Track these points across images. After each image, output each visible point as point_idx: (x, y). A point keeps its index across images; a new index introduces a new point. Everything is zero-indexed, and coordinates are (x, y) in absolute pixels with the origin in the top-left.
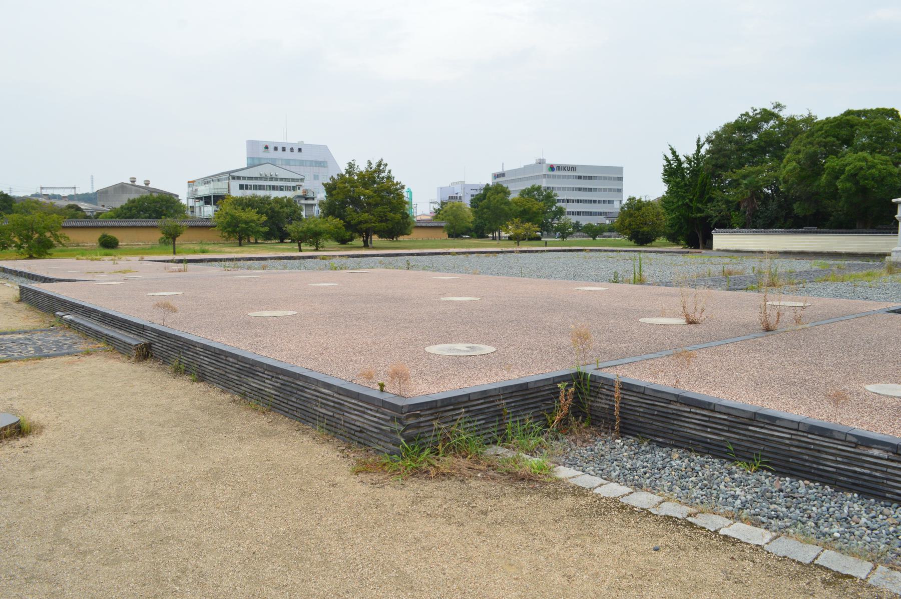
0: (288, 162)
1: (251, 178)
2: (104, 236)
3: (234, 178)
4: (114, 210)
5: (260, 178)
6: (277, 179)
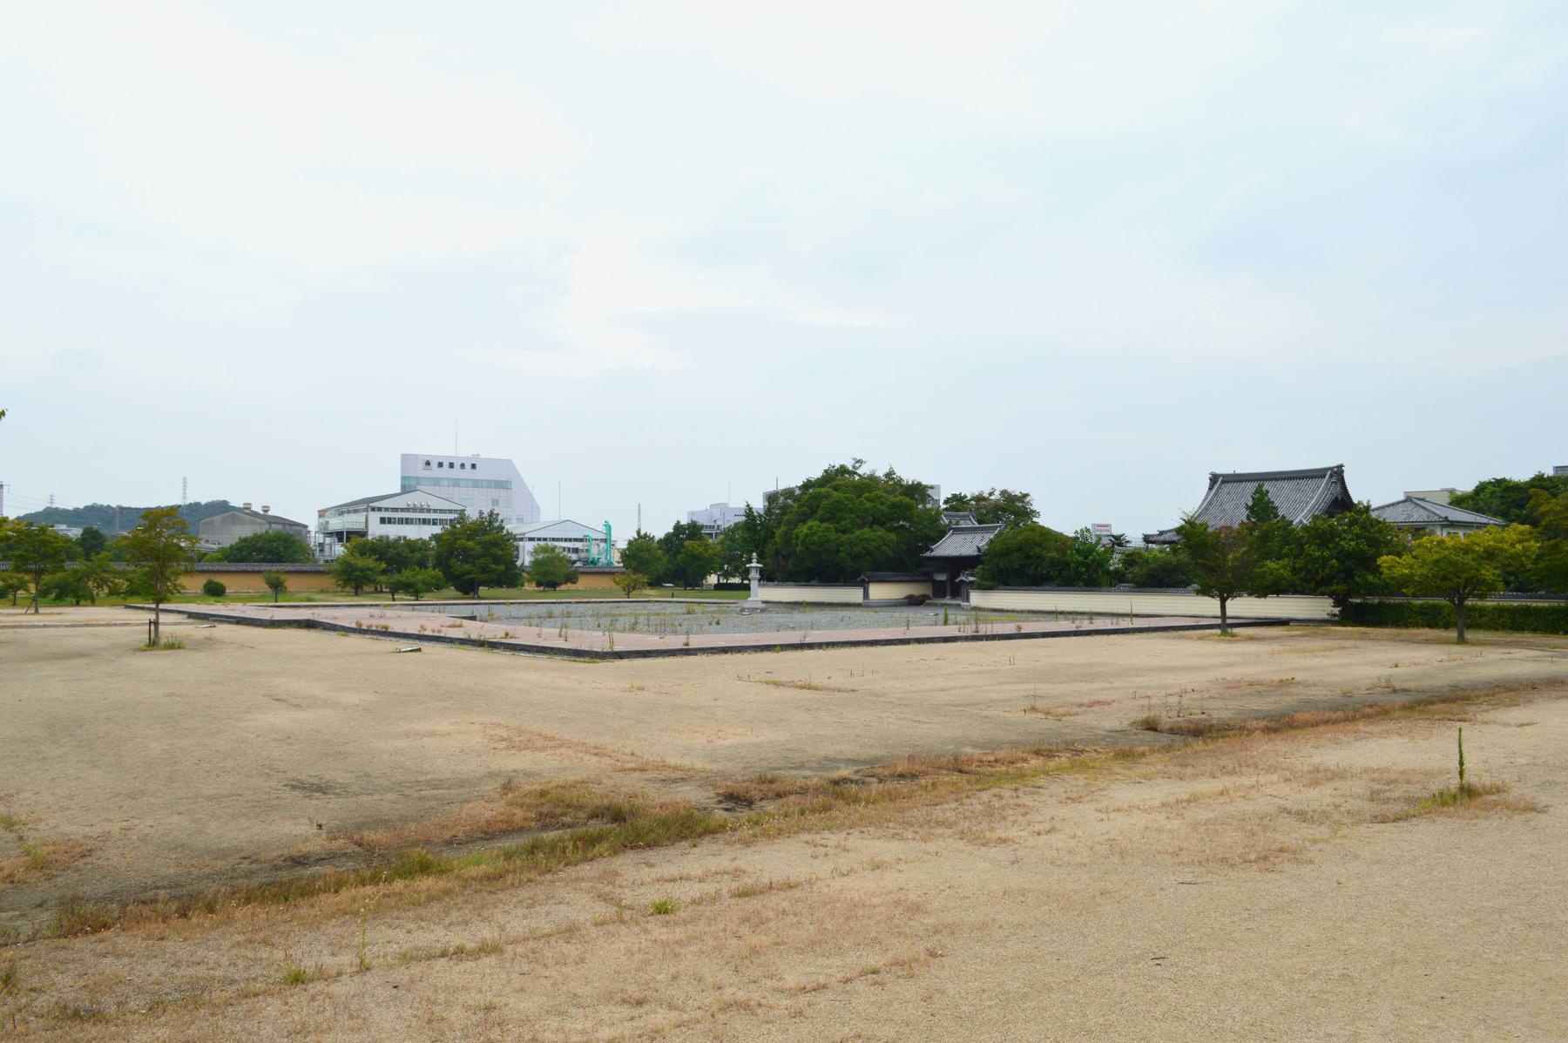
0: (456, 483)
1: (395, 510)
2: (210, 583)
3: (373, 509)
4: (220, 550)
5: (407, 510)
6: (429, 511)
